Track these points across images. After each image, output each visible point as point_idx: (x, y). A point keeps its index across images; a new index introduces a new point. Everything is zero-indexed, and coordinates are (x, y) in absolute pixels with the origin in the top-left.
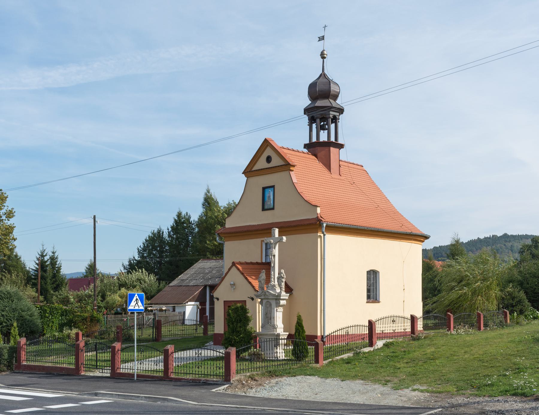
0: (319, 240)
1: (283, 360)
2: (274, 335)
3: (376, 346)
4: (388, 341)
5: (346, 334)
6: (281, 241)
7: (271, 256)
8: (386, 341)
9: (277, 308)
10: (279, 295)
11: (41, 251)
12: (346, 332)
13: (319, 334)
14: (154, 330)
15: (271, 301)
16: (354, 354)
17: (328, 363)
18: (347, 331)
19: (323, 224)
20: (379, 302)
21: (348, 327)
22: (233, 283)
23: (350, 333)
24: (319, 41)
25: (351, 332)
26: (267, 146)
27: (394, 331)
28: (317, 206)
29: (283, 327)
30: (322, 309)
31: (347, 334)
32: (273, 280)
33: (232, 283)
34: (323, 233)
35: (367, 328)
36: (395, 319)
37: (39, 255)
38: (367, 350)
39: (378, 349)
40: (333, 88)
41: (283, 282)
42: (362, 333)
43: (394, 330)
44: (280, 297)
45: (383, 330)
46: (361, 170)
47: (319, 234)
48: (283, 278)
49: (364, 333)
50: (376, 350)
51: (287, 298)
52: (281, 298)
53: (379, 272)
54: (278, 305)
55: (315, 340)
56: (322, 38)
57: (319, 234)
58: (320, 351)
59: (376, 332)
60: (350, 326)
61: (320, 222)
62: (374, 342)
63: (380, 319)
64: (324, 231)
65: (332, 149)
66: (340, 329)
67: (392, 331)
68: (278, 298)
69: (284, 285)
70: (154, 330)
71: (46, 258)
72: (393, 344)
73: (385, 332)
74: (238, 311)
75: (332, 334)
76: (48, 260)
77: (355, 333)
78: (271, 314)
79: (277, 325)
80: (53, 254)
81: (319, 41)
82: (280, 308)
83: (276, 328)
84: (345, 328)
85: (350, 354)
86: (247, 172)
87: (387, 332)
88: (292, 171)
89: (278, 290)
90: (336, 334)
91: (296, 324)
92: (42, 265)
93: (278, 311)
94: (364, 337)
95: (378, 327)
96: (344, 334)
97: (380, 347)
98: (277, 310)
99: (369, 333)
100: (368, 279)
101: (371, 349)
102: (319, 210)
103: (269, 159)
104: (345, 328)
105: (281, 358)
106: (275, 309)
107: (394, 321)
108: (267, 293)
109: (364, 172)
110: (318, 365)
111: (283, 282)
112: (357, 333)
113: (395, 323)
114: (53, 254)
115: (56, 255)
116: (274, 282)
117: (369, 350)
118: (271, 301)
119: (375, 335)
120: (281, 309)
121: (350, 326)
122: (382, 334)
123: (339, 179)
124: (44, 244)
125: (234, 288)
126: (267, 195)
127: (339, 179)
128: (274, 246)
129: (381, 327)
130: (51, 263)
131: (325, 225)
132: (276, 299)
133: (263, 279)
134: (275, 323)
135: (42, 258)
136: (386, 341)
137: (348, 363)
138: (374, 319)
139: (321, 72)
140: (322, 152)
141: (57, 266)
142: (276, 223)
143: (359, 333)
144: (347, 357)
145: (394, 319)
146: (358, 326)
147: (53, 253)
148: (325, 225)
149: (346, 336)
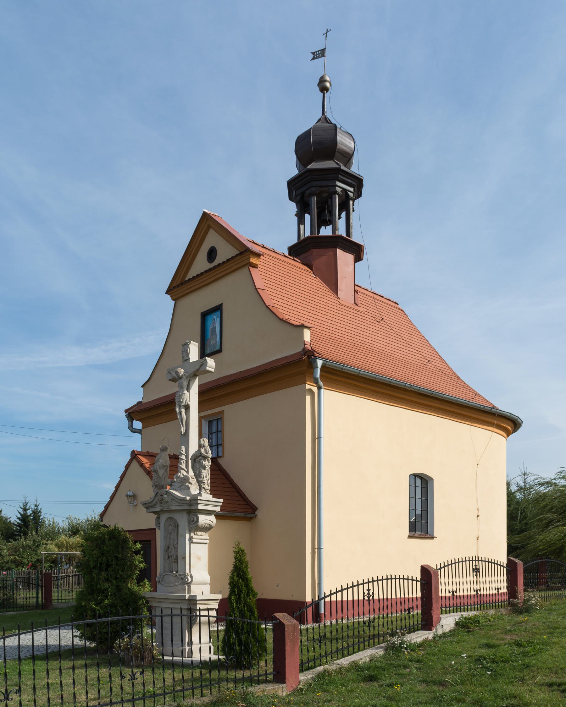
0: (308, 398)
1: (203, 664)
2: (183, 599)
3: (439, 627)
4: (465, 614)
5: (366, 598)
6: (202, 369)
7: (180, 408)
8: (462, 616)
9: (192, 534)
10: (195, 500)
11: (23, 504)
12: (366, 592)
13: (309, 599)
14: (40, 592)
15: (176, 516)
16: (386, 649)
17: (313, 679)
18: (369, 590)
19: (316, 362)
20: (432, 538)
21: (371, 580)
22: (131, 494)
23: (376, 597)
24: (313, 59)
25: (362, 253)
26: (209, 227)
27: (477, 594)
28: (303, 326)
29: (209, 582)
30: (316, 546)
31: (369, 599)
32: (183, 466)
33: (130, 493)
34: (316, 382)
35: (419, 584)
36: (480, 565)
37: (21, 508)
38: (418, 637)
39: (444, 635)
40: (343, 141)
41: (204, 468)
42: (406, 596)
43: (477, 590)
44: (197, 504)
45: (455, 590)
46: (395, 307)
47: (308, 387)
48: (205, 458)
49: (410, 596)
50: (440, 637)
51: (218, 509)
52: (200, 507)
53: (432, 479)
54: (194, 527)
55: (276, 615)
56: (320, 54)
57: (308, 387)
58: (288, 647)
59: (440, 595)
60: (375, 579)
61: (309, 357)
62: (434, 619)
63: (448, 565)
64: (318, 376)
65: (340, 253)
66: (350, 585)
67: (473, 593)
68: (193, 508)
69: (209, 477)
70: (40, 592)
71: (29, 512)
72: (479, 622)
73: (458, 594)
74: (103, 542)
75: (328, 599)
76: (31, 514)
77: (389, 597)
78: (176, 548)
79: (191, 576)
80: (35, 508)
81: (313, 59)
82: (199, 533)
83: (189, 584)
84: (363, 584)
85: (378, 652)
86: (178, 286)
87: (462, 594)
88: (255, 266)
89: (194, 490)
90: (339, 599)
91: (233, 571)
92: (24, 519)
93: (194, 540)
94: (411, 606)
95: (443, 584)
96: (361, 598)
97: (447, 630)
98: (191, 539)
99: (422, 598)
100: (412, 487)
101: (429, 635)
102: (307, 335)
103: (212, 254)
104: (363, 584)
105: (196, 657)
106: (188, 536)
107: (476, 570)
108: (165, 496)
109: (402, 312)
110: (282, 690)
111: (204, 468)
112: (394, 597)
113: (478, 574)
114: (35, 508)
115: (39, 508)
116: (188, 472)
117: (423, 637)
118: (176, 516)
119: (437, 602)
120: (202, 537)
121: (375, 579)
122: (451, 599)
123: (353, 309)
124: (26, 496)
125: (135, 503)
126: (209, 326)
127: (353, 309)
128: (185, 384)
129: (451, 584)
130: (34, 518)
131: (320, 363)
132: (189, 512)
133: (164, 466)
134: (187, 571)
135: (25, 512)
136: (462, 616)
137: (371, 679)
138: (433, 564)
139: (320, 115)
140: (321, 260)
141: (40, 521)
142: (224, 377)
143: (398, 596)
144: (368, 660)
145: (476, 566)
146: (391, 579)
147: (36, 506)
148: (320, 363)
149: (366, 603)
